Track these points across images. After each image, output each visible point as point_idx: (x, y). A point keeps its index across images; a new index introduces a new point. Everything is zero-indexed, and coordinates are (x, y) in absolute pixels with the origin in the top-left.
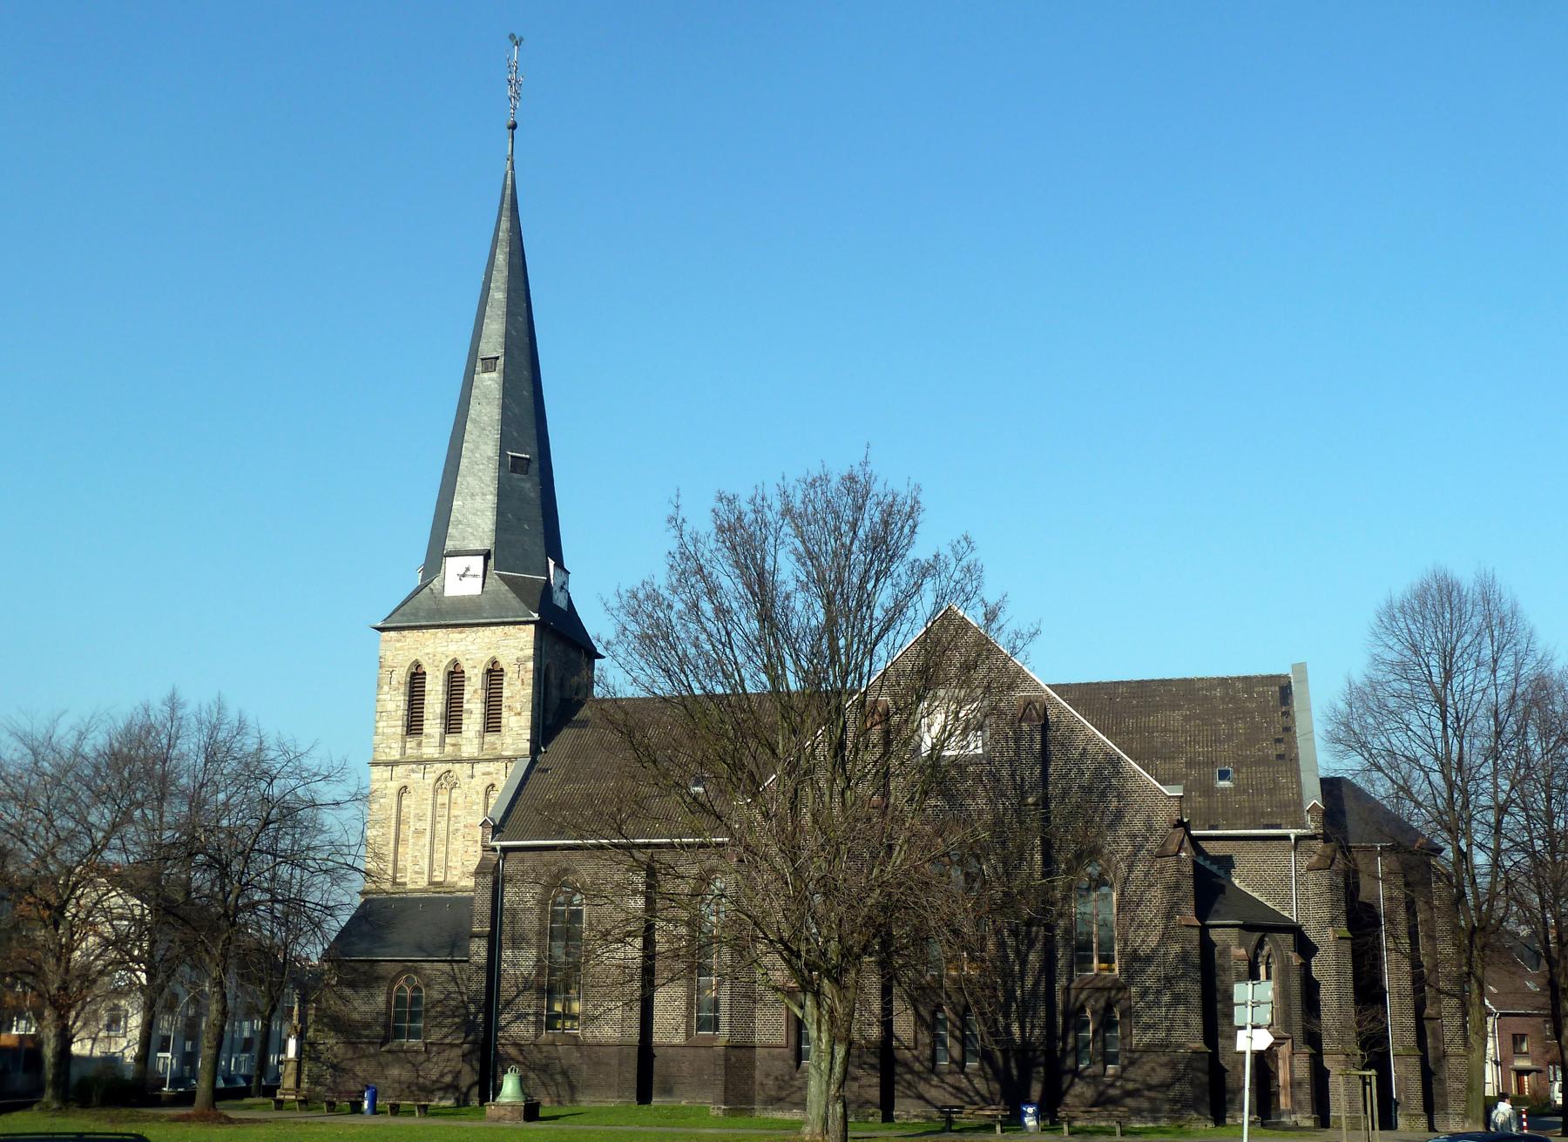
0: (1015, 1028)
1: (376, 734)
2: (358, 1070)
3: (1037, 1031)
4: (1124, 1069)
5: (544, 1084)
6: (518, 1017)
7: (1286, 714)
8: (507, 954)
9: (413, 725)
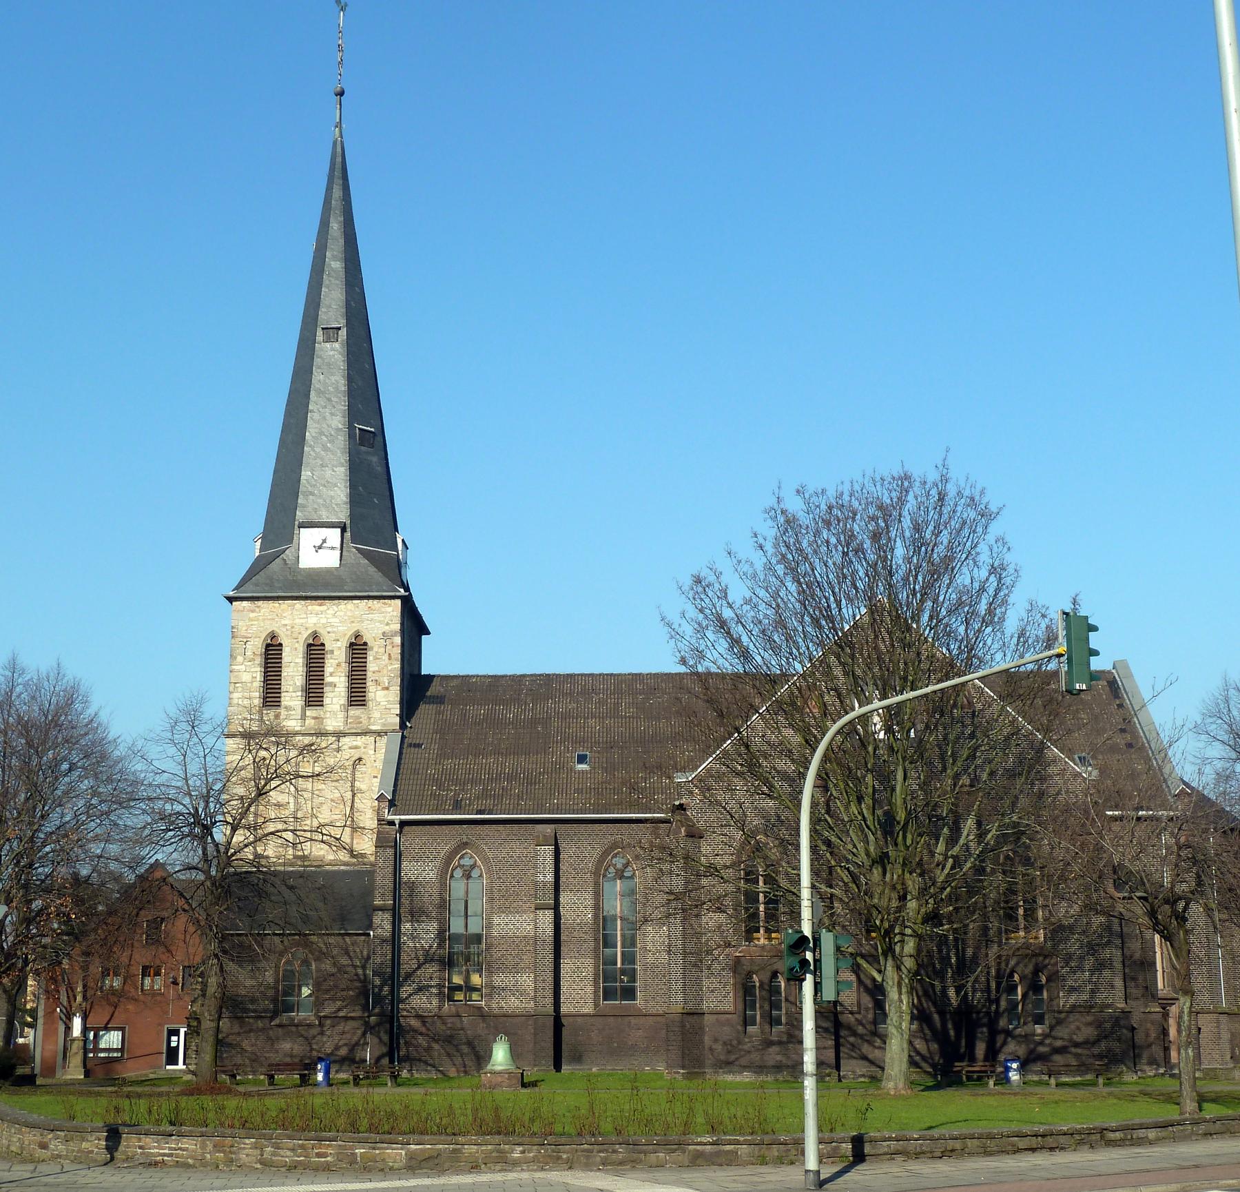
0: (952, 993)
1: (230, 705)
2: (246, 1044)
3: (978, 995)
4: (1052, 1028)
5: (449, 1055)
6: (420, 989)
7: (1120, 706)
8: (406, 927)
9: (271, 694)
